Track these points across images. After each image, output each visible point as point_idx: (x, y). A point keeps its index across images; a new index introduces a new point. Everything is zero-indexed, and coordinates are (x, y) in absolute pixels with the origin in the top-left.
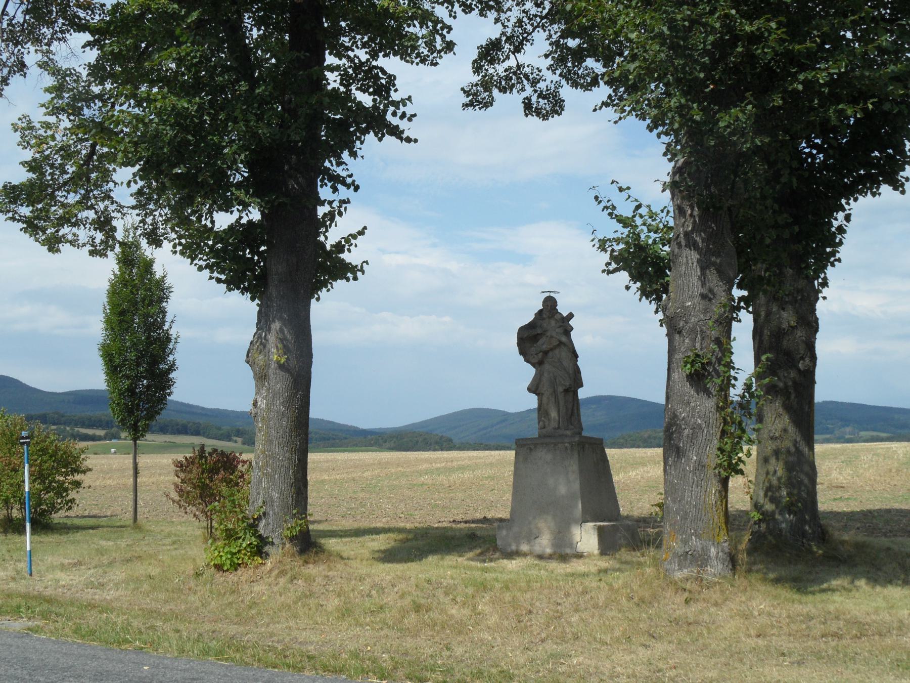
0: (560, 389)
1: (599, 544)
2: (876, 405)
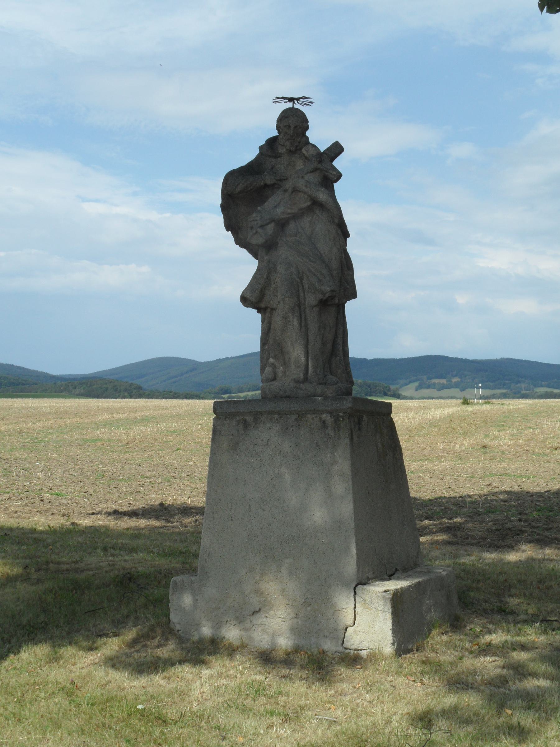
0: (311, 299)
1: (395, 631)
2: (551, 362)
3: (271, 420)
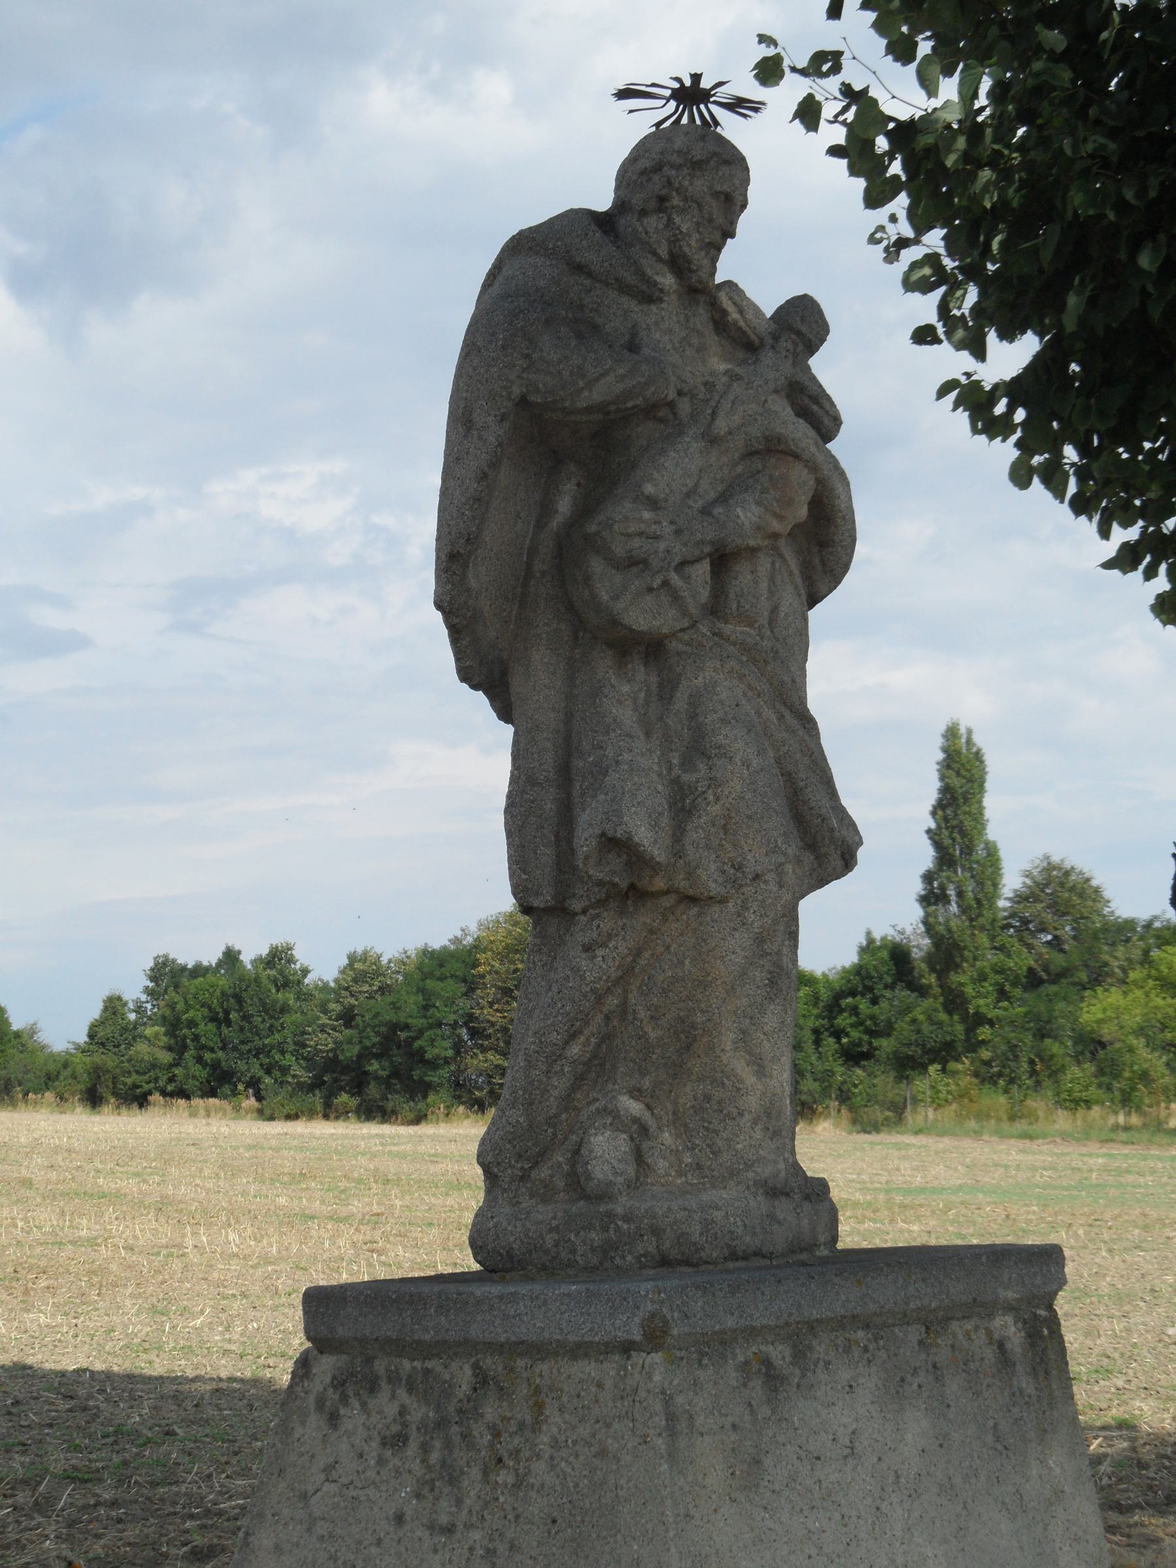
3: (847, 1350)
